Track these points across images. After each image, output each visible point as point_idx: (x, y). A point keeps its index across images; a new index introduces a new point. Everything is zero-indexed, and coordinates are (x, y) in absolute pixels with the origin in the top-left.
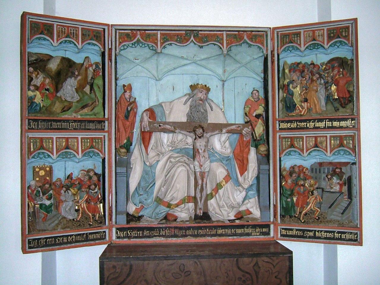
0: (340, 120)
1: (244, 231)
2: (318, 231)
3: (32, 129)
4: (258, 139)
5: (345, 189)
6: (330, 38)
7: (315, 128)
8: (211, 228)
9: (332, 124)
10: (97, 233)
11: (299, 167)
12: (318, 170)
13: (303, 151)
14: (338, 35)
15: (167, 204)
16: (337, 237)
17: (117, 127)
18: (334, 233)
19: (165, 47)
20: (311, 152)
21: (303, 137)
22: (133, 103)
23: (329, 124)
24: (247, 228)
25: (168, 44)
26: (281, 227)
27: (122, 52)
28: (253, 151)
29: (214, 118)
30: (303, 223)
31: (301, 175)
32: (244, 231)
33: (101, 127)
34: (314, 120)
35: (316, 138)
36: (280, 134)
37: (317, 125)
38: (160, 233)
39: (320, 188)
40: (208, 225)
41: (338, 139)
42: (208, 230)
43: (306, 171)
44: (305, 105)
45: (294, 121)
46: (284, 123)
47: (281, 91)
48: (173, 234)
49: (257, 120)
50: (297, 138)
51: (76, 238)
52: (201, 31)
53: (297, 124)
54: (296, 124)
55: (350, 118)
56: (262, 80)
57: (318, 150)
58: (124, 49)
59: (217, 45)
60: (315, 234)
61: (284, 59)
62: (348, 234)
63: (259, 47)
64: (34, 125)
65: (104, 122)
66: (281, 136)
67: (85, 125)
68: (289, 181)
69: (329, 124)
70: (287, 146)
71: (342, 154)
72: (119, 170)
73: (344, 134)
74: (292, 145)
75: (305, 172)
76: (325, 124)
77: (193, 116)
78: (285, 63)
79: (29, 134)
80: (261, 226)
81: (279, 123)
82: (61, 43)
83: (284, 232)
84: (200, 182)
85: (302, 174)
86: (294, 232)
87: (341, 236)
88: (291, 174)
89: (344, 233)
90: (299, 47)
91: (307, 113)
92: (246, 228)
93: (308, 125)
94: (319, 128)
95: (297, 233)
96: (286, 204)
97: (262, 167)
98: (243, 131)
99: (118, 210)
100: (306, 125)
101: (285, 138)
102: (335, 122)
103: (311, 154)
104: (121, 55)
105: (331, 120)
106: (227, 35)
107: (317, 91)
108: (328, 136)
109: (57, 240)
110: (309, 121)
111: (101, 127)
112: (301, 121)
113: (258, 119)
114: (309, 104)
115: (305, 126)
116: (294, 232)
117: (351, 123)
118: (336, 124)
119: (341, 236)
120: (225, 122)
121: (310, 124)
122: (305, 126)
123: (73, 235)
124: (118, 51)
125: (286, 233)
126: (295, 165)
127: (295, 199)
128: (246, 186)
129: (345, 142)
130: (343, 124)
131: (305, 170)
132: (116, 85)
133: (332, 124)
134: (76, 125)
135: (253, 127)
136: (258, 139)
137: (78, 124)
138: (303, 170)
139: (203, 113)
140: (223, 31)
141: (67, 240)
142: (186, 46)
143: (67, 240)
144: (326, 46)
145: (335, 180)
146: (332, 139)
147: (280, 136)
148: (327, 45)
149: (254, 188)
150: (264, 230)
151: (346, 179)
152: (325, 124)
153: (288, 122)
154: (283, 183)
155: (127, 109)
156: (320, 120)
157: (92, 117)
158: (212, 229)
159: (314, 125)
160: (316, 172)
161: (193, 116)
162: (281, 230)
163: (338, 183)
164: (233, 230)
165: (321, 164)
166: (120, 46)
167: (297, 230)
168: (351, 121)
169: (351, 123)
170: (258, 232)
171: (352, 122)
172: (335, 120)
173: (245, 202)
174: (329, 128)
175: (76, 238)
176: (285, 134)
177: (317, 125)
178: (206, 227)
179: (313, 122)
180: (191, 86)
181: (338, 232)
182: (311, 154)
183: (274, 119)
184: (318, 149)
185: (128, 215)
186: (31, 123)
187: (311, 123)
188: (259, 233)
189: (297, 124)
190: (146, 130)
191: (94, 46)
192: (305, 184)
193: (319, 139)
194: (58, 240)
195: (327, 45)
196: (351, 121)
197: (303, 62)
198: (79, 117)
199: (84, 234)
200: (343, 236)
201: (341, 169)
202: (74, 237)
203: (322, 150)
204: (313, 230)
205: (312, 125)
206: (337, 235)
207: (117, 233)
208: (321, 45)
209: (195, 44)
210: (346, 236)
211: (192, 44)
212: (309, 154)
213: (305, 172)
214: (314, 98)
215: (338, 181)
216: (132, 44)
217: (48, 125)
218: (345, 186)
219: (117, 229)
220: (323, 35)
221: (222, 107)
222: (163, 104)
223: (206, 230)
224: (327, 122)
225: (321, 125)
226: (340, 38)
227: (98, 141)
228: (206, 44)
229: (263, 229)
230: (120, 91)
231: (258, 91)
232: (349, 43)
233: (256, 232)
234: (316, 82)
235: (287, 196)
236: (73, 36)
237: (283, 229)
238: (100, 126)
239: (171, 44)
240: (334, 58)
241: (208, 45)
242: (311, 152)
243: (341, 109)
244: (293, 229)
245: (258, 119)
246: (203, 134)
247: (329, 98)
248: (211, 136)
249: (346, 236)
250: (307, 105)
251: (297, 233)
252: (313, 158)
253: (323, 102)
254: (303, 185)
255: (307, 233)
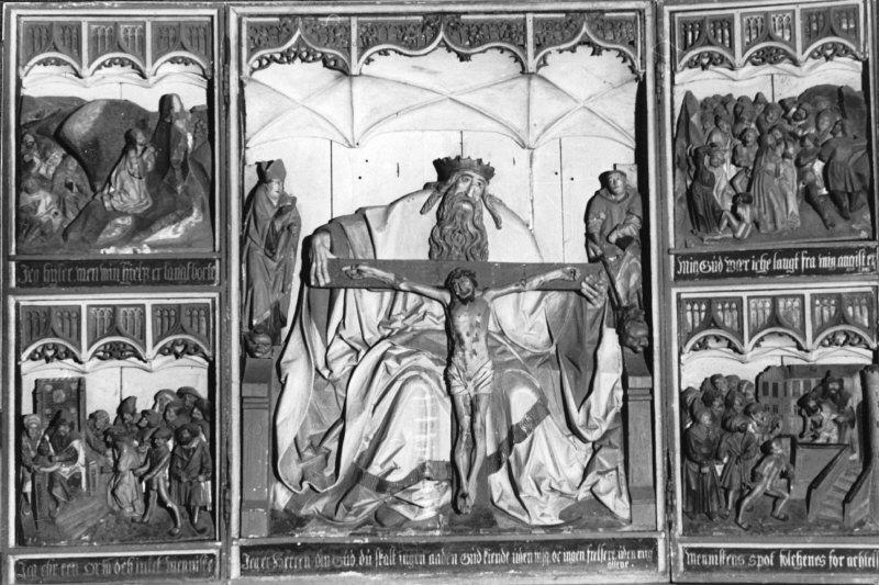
0: (836, 253)
1: (586, 557)
2: (785, 552)
3: (28, 285)
4: (625, 304)
5: (853, 433)
6: (810, 37)
7: (772, 273)
8: (495, 547)
9: (817, 262)
10: (192, 557)
11: (729, 378)
12: (780, 388)
13: (743, 337)
14: (832, 30)
15: (375, 483)
16: (836, 565)
17: (244, 275)
18: (827, 556)
19: (369, 61)
20: (762, 339)
21: (741, 298)
22: (286, 207)
23: (808, 262)
24: (594, 548)
25: (379, 53)
26: (686, 545)
27: (257, 75)
28: (610, 337)
29: (504, 247)
30: (746, 530)
31: (737, 402)
32: (586, 557)
33: (206, 276)
34: (769, 254)
35: (774, 299)
36: (679, 290)
37: (779, 264)
38: (357, 562)
39: (787, 436)
40: (488, 538)
41: (833, 302)
42: (486, 553)
43: (749, 391)
44: (745, 212)
45: (717, 254)
46: (690, 261)
47: (678, 171)
48: (393, 563)
49: (619, 251)
50: (724, 300)
51: (135, 566)
52: (466, 13)
53: (725, 264)
54: (721, 263)
55: (862, 248)
56: (633, 145)
57: (781, 335)
58: (261, 67)
59: (509, 50)
60: (776, 560)
61: (688, 87)
62: (863, 555)
63: (621, 54)
64: (32, 275)
65: (214, 264)
66: (683, 296)
67: (162, 273)
68: (706, 419)
69: (808, 262)
70: (697, 325)
71: (841, 342)
72: (249, 390)
73: (849, 290)
74: (713, 320)
75: (745, 394)
76: (800, 263)
77: (447, 245)
78: (689, 96)
79: (19, 298)
80: (633, 544)
81: (676, 260)
82: (99, 68)
83: (694, 560)
84: (466, 420)
85: (737, 398)
86: (722, 557)
87: (845, 561)
88: (707, 400)
89: (854, 552)
90: (727, 55)
91: (750, 235)
92: (591, 549)
93: (754, 267)
94: (782, 272)
95: (730, 560)
96: (697, 482)
97: (636, 382)
98: (584, 284)
99: (246, 498)
100: (750, 265)
101: (693, 301)
102: (825, 259)
103: (761, 343)
104: (256, 81)
105: (812, 252)
106: (536, 23)
107: (777, 174)
108: (807, 294)
109: (86, 568)
110: (757, 254)
111: (206, 276)
112: (735, 255)
113: (624, 250)
114: (756, 210)
115: (746, 269)
116: (722, 557)
117: (866, 259)
118: (827, 262)
119: (845, 561)
120: (536, 260)
121: (759, 265)
122: (746, 269)
123: (126, 558)
124: (246, 70)
125: (701, 560)
126: (719, 376)
127: (719, 469)
128: (593, 436)
129: (850, 309)
130: (846, 261)
131: (747, 388)
132: (244, 164)
133: (817, 262)
134: (137, 273)
135: (612, 272)
136: (625, 304)
137: (142, 272)
138: (739, 388)
139: (473, 238)
140: (525, 12)
141: (113, 572)
142: (426, 54)
143: (113, 572)
144: (799, 56)
145: (826, 414)
146: (818, 302)
147: (678, 294)
148: (803, 53)
149: (616, 439)
150: (641, 554)
151: (855, 409)
152: (800, 263)
153: (699, 257)
154: (688, 425)
155: (272, 224)
156: (788, 253)
157: (181, 250)
158: (498, 551)
159: (771, 266)
160: (775, 393)
161: (447, 245)
162: (685, 556)
163: (835, 420)
164: (554, 553)
165: (788, 371)
166: (251, 62)
167: (729, 551)
168: (867, 255)
169: (866, 259)
170: (624, 561)
171: (869, 258)
172: (825, 252)
173: (574, 329)
174: (809, 272)
175: (135, 566)
176: (691, 292)
177: (779, 264)
178: (483, 545)
179: (766, 258)
180: (438, 164)
181: (839, 552)
182: (761, 343)
183: (664, 250)
184: (781, 330)
185: (273, 514)
186: (25, 271)
187: (762, 261)
188: (627, 563)
189: (725, 264)
190: (322, 284)
191: (186, 64)
192: (747, 426)
193: (781, 303)
194: (90, 568)
195: (803, 53)
196: (867, 255)
197: (736, 97)
198: (147, 251)
199: (155, 557)
200: (851, 562)
201: (841, 382)
202: (130, 564)
203: (791, 333)
204: (774, 550)
205: (764, 264)
206: (835, 561)
207: (242, 560)
208: (785, 52)
209: (449, 50)
210: (857, 561)
211: (443, 50)
212: (757, 345)
213: (745, 394)
214: (771, 195)
215: (834, 416)
216: (282, 54)
217: (66, 273)
218: (853, 427)
219: (243, 549)
220: (791, 27)
221: (527, 217)
222: (368, 213)
223: (482, 553)
224: (803, 259)
225: (789, 264)
226: (836, 35)
227: (700, 306)
228: (480, 49)
229: (639, 552)
230: (252, 177)
231: (623, 174)
232: (858, 49)
233: (618, 560)
234: (774, 150)
235: (699, 458)
236: (133, 48)
237: (691, 550)
238: (203, 273)
239: (385, 53)
240: (817, 87)
241: (484, 51)
242: (762, 339)
243: (841, 225)
244: (719, 549)
245: (624, 250)
246: (473, 293)
247: (807, 196)
248: (496, 297)
249: (857, 561)
250: (752, 213)
251: (730, 560)
252: (767, 357)
253: (793, 206)
254: (743, 430)
255: (757, 559)
